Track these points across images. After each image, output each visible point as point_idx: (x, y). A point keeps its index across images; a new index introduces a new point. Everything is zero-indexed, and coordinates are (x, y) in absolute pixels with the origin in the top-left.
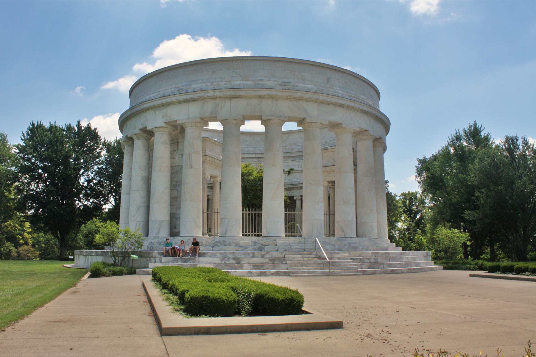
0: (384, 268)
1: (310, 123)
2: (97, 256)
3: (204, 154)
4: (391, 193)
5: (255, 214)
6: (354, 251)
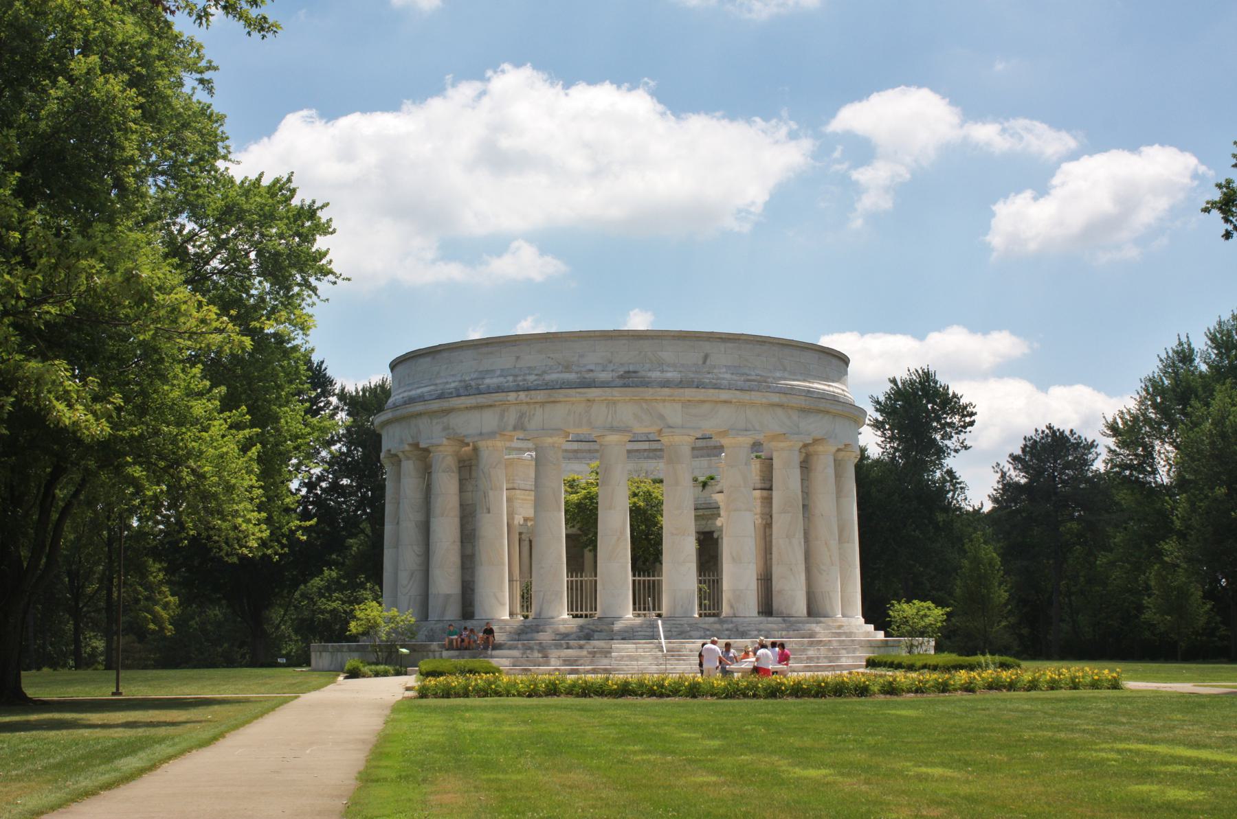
2: (350, 651)
3: (511, 486)
5: (577, 581)
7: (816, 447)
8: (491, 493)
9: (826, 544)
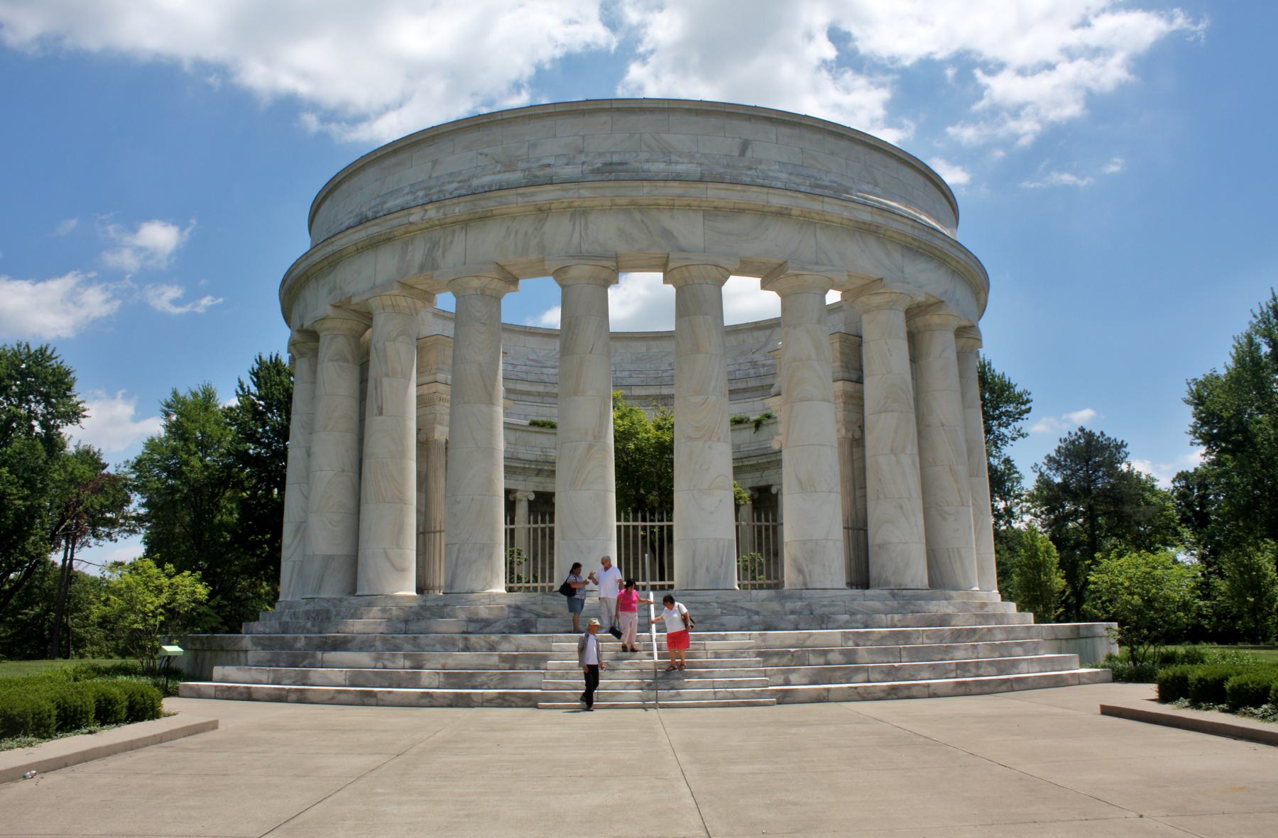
0: (869, 682)
1: (684, 269)
4: (1140, 474)
5: (543, 530)
6: (818, 627)
7: (927, 317)
8: (386, 382)
9: (951, 469)
